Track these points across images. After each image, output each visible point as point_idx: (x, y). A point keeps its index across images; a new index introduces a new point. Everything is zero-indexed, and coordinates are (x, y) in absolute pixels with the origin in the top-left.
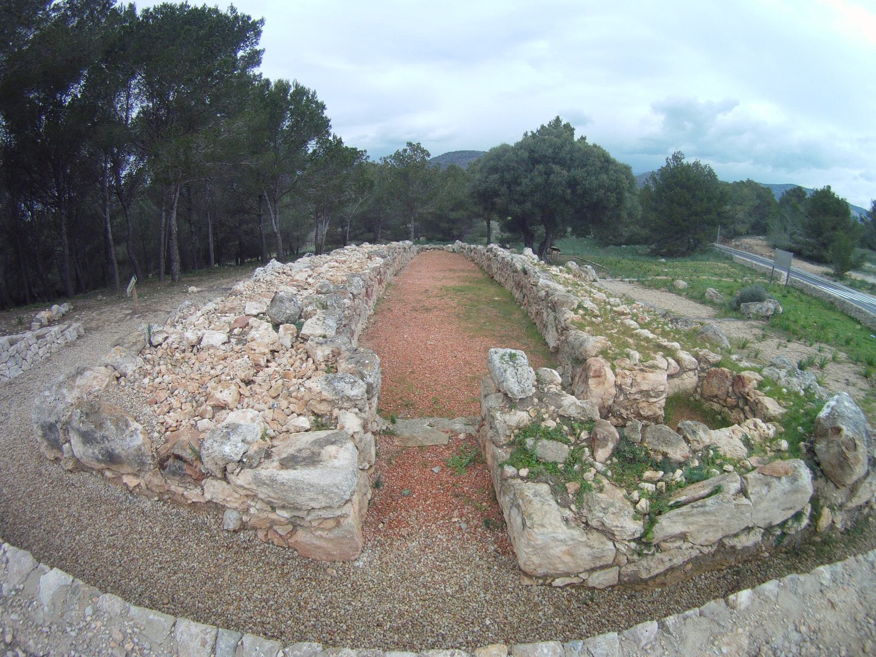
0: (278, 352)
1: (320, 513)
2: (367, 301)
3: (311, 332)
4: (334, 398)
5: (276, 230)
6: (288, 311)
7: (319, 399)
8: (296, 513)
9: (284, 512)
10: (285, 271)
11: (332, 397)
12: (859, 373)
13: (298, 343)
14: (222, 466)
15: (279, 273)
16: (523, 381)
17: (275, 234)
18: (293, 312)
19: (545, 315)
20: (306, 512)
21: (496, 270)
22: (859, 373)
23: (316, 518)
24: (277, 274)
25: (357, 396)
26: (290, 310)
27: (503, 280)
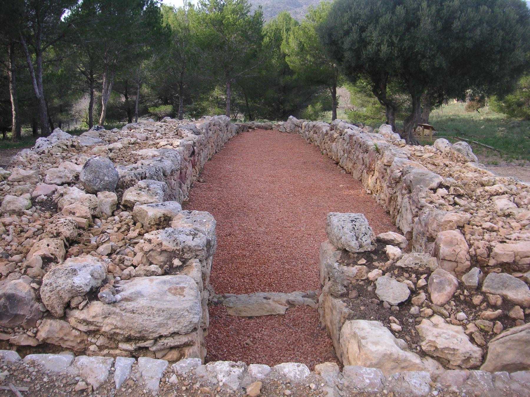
0: (98, 218)
1: (166, 341)
2: (181, 184)
3: (136, 198)
4: (175, 248)
5: (38, 95)
6: (106, 178)
7: (159, 250)
8: (142, 344)
9: (128, 345)
10: (75, 144)
11: (173, 248)
12: (354, 136)
13: (120, 210)
14: (66, 300)
15: (67, 146)
16: (361, 235)
17: (38, 100)
18: (111, 179)
19: (399, 199)
20: (152, 341)
21: (342, 153)
22: (354, 136)
23: (162, 347)
24: (65, 147)
25: (199, 246)
26: (108, 177)
27: (350, 165)
